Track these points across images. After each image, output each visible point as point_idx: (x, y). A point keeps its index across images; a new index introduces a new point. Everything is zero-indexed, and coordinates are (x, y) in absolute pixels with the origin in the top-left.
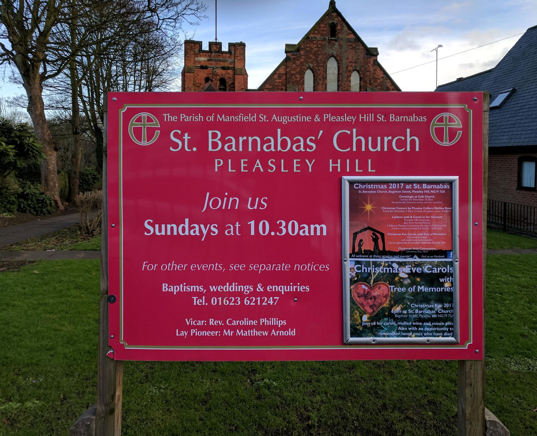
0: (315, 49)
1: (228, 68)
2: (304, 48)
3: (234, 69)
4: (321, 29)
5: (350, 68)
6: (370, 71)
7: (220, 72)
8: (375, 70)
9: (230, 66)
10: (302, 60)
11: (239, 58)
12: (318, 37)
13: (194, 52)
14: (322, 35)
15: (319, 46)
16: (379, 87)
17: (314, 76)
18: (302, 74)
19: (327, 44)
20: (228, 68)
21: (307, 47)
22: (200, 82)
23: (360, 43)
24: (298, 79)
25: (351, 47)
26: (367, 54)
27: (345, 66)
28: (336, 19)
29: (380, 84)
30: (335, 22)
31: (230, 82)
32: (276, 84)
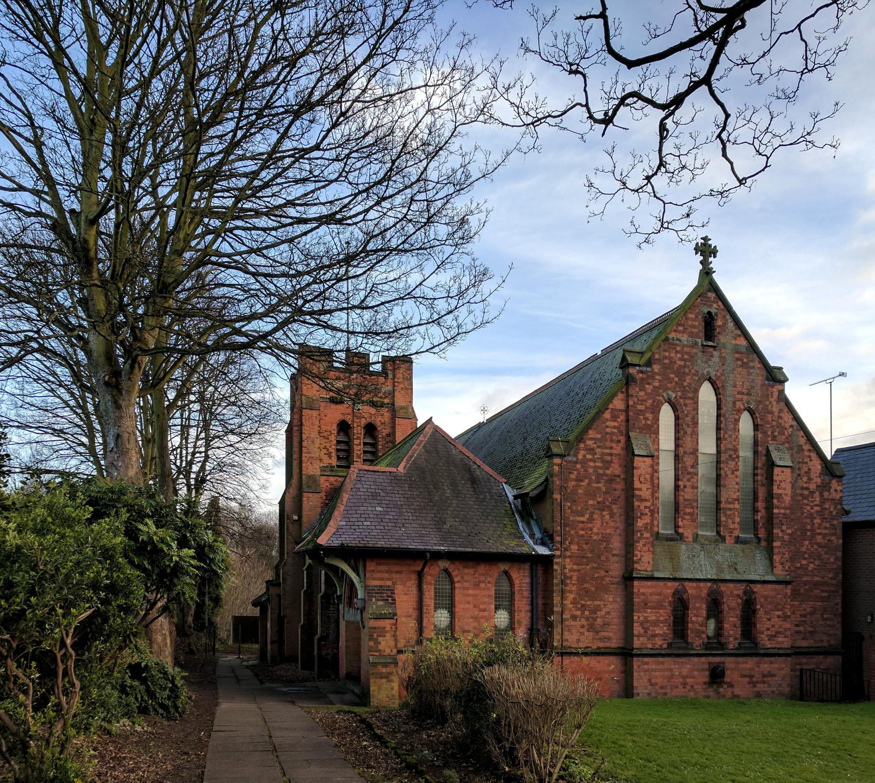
4: (690, 323)
5: (739, 405)
6: (772, 413)
8: (781, 411)
10: (657, 384)
11: (401, 386)
12: (684, 338)
14: (691, 335)
15: (686, 357)
16: (787, 445)
17: (677, 418)
18: (656, 411)
19: (700, 354)
21: (665, 357)
22: (328, 428)
24: (649, 422)
25: (740, 363)
26: (767, 379)
27: (730, 399)
28: (715, 306)
30: (713, 311)
31: (385, 432)
32: (608, 430)
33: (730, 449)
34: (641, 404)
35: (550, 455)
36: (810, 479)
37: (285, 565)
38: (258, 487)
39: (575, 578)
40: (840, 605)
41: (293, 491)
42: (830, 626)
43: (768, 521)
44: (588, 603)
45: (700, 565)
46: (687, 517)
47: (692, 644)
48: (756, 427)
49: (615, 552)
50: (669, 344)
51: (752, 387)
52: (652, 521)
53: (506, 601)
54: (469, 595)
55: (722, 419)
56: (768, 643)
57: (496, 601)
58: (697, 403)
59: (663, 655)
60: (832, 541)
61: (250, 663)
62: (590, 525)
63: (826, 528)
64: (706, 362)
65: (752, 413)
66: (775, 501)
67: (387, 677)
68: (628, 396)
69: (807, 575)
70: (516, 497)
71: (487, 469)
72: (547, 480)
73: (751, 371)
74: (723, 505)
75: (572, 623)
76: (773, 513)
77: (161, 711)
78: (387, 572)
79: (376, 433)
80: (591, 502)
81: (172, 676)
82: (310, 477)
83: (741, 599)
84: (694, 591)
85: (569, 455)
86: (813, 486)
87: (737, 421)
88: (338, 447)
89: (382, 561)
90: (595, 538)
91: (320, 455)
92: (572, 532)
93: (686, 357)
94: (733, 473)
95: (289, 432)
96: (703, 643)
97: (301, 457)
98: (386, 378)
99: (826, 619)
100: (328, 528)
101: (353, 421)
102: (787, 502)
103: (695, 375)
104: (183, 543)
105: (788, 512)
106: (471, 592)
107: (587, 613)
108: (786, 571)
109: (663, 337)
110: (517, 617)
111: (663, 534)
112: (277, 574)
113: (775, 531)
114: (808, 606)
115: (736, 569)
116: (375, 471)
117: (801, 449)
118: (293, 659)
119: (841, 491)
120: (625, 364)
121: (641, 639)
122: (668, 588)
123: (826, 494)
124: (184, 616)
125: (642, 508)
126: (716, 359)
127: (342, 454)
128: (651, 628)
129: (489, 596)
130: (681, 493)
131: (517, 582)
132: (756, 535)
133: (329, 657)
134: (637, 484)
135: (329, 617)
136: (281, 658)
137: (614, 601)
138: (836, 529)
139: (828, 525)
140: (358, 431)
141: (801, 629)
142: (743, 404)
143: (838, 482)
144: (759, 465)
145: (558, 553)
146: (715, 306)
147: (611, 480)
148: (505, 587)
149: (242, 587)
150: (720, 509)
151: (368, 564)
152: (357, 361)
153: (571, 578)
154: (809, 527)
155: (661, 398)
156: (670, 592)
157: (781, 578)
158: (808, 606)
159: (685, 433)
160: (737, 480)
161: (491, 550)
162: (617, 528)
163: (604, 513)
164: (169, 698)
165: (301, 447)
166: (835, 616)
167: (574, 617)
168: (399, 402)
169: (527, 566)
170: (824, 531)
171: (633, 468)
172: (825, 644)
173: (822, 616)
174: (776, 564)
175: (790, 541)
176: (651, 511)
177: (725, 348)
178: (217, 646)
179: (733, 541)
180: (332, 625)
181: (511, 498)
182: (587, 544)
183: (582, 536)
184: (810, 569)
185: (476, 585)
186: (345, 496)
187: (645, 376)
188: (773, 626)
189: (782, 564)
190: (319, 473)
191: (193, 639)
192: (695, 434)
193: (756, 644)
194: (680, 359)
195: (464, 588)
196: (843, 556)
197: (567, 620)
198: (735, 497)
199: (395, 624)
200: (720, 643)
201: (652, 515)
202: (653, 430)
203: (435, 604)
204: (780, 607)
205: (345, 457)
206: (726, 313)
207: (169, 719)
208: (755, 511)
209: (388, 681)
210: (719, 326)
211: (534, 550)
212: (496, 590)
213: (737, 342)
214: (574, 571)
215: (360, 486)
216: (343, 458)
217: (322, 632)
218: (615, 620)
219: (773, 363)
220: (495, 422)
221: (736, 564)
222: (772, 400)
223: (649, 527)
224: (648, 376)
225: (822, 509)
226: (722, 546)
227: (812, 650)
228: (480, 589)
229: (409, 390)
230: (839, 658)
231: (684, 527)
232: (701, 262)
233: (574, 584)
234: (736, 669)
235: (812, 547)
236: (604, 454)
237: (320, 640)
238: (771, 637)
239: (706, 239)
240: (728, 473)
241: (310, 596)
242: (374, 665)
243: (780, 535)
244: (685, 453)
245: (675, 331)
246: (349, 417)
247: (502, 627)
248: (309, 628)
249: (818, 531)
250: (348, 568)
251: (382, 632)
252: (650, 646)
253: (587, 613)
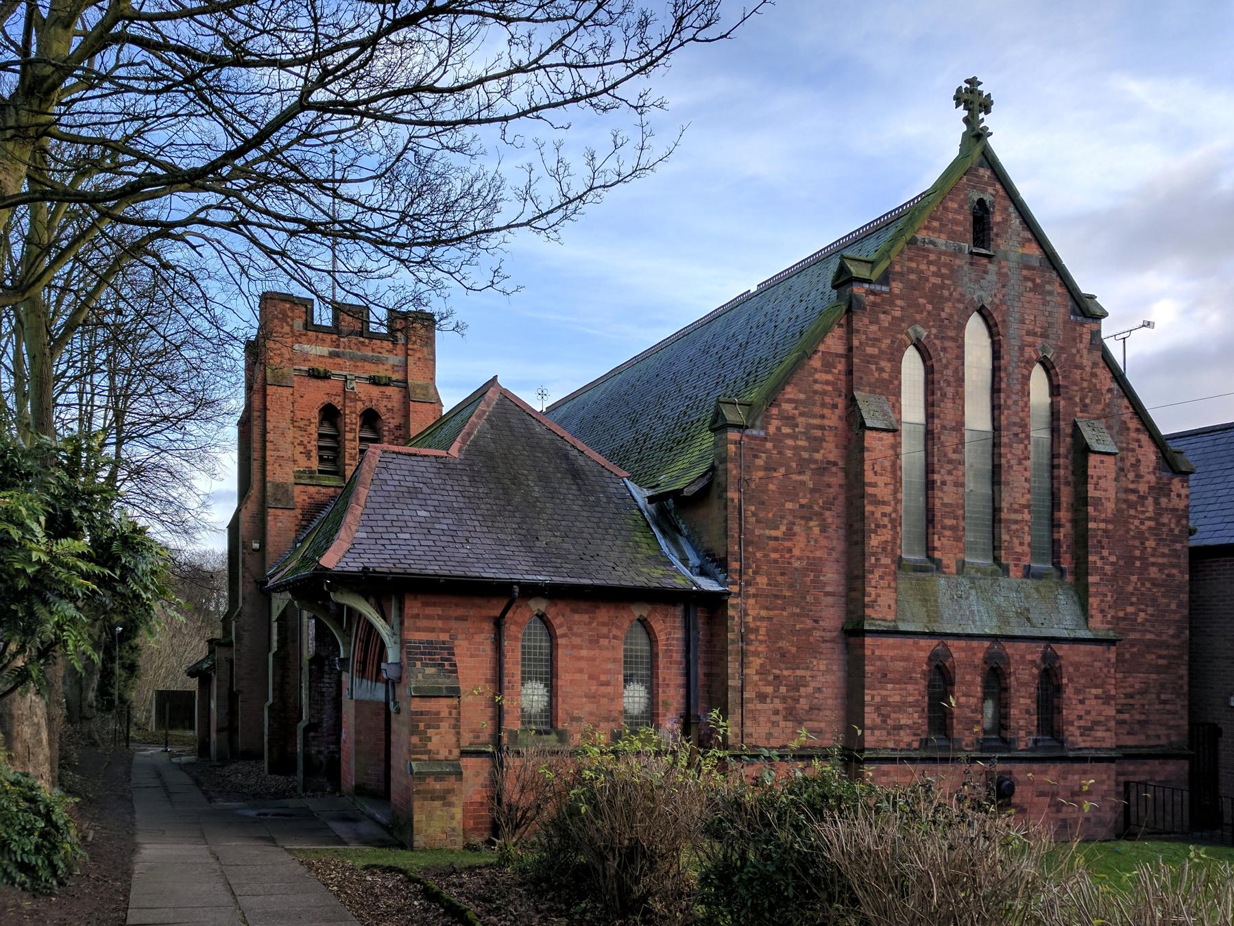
0: (933, 280)
1: (388, 383)
2: (902, 274)
3: (404, 385)
4: (950, 216)
5: (1029, 352)
6: (1080, 367)
7: (363, 390)
8: (1095, 365)
9: (394, 377)
10: (897, 313)
11: (418, 355)
12: (941, 241)
13: (292, 326)
14: (952, 236)
15: (944, 271)
19: (966, 268)
20: (388, 383)
21: (911, 271)
22: (307, 415)
23: (1054, 274)
24: (885, 376)
25: (1030, 284)
26: (1074, 312)
27: (1015, 343)
28: (990, 190)
30: (987, 198)
31: (394, 422)
32: (817, 387)
33: (1015, 424)
34: (873, 346)
35: (719, 425)
37: (239, 615)
38: (195, 505)
39: (763, 631)
40: (1186, 679)
41: (252, 506)
42: (1169, 712)
43: (1076, 542)
44: (786, 673)
45: (975, 609)
46: (948, 533)
47: (960, 741)
48: (1055, 390)
49: (828, 589)
50: (919, 249)
51: (1050, 325)
52: (894, 539)
53: (646, 670)
54: (580, 659)
55: (1003, 375)
56: (1080, 739)
57: (625, 669)
58: (961, 347)
59: (912, 760)
60: (1173, 576)
61: (184, 759)
62: (788, 544)
63: (1163, 555)
64: (977, 281)
65: (1048, 367)
66: (1091, 509)
67: (444, 797)
68: (850, 331)
69: (1134, 630)
70: (651, 500)
71: (595, 456)
72: (712, 468)
73: (1048, 298)
74: (1004, 515)
75: (759, 706)
76: (1087, 529)
77: (21, 877)
78: (440, 617)
79: (379, 424)
80: (789, 505)
81: (47, 806)
82: (278, 486)
83: (1037, 666)
84: (963, 654)
85: (753, 427)
86: (1143, 488)
87: (1026, 379)
88: (321, 444)
89: (432, 599)
90: (797, 564)
91: (292, 455)
92: (759, 555)
93: (944, 271)
94: (1020, 464)
95: (245, 425)
96: (978, 740)
97: (264, 457)
98: (395, 343)
99: (1165, 702)
100: (336, 543)
101: (344, 405)
102: (1109, 511)
103: (959, 301)
105: (1110, 527)
106: (584, 653)
107: (783, 689)
108: (1108, 623)
109: (908, 236)
110: (661, 696)
111: (907, 560)
113: (1091, 558)
114: (1135, 681)
115: (1028, 619)
116: (410, 455)
117: (1124, 428)
118: (253, 755)
119: (1187, 496)
120: (843, 279)
121: (877, 733)
122: (921, 649)
123: (1164, 501)
124: (81, 690)
125: (878, 515)
126: (992, 277)
127: (326, 454)
128: (893, 715)
129: (615, 661)
130: (938, 493)
131: (661, 637)
132: (1057, 565)
133: (321, 757)
134: (869, 477)
135: (322, 694)
136: (232, 754)
137: (828, 671)
138: (1179, 557)
139: (1166, 551)
140: (352, 420)
141: (1126, 716)
142: (1036, 351)
143: (1183, 481)
144: (1062, 451)
145: (735, 589)
146: (990, 190)
147: (823, 469)
148: (641, 645)
149: (170, 648)
150: (1000, 521)
151: (408, 603)
153: (757, 630)
154: (1137, 553)
155: (904, 336)
156: (924, 655)
157: (1101, 635)
158: (1135, 681)
159: (944, 395)
160: (1027, 474)
161: (623, 583)
162: (833, 549)
163: (812, 524)
164: (38, 849)
165: (264, 442)
166: (1178, 696)
167: (762, 697)
168: (415, 378)
169: (679, 611)
170: (1160, 560)
171: (862, 449)
172: (1163, 741)
173: (1159, 697)
174: (1093, 612)
175: (1114, 575)
176: (892, 521)
177: (1007, 259)
178: (132, 734)
179: (1019, 574)
180: (328, 708)
181: (642, 502)
182: (782, 574)
183: (776, 561)
184: (1139, 620)
185: (594, 642)
186: (363, 492)
187: (878, 300)
188: (1088, 713)
189: (1102, 611)
190: (292, 480)
191: (95, 725)
192: (959, 397)
193: (1062, 742)
194: (935, 274)
195: (574, 647)
196: (1191, 600)
197: (751, 700)
198: (1023, 501)
199: (457, 708)
200: (1004, 740)
201: (894, 527)
202: (891, 387)
203: (523, 672)
204: (1098, 682)
205: (332, 455)
206: (1008, 203)
207: (35, 893)
208: (1054, 525)
209: (444, 805)
210: (998, 223)
211: (695, 584)
212: (625, 650)
213: (1026, 251)
214: (762, 619)
215: (385, 476)
216: (328, 460)
217: (311, 716)
218: (830, 702)
219: (1084, 288)
220: (564, 408)
221: (1028, 610)
222: (1081, 346)
223: (889, 548)
224: (883, 300)
225: (1158, 524)
226: (1003, 581)
227: (1144, 751)
228: (600, 648)
229: (430, 361)
230: (1185, 765)
231: (943, 548)
232: (966, 120)
233: (761, 642)
234: (1030, 779)
235: (1143, 585)
236: (810, 427)
237: (306, 730)
238: (1085, 731)
239: (973, 82)
240: (1013, 462)
241: (283, 660)
242: (422, 776)
243: (1099, 564)
244: (944, 427)
245: (926, 228)
246: (339, 399)
247: (636, 712)
248: (285, 713)
249: (1152, 560)
250: (372, 610)
251: (434, 720)
252: (891, 745)
253: (783, 689)
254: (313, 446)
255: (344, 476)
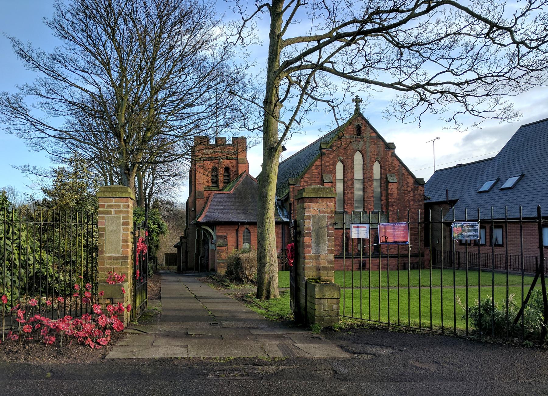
5: (373, 159)
8: (393, 160)
14: (350, 134)
16: (396, 174)
17: (344, 167)
18: (334, 165)
26: (386, 148)
29: (397, 171)
31: (234, 170)
36: (408, 186)
41: (192, 198)
66: (389, 196)
82: (200, 192)
86: (409, 189)
91: (204, 180)
104: (154, 224)
112: (185, 233)
120: (321, 148)
123: (416, 192)
152: (221, 142)
168: (240, 157)
169: (281, 226)
180: (206, 252)
202: (334, 172)
208: (381, 200)
234: (371, 262)
240: (368, 186)
241: (198, 241)
242: (219, 263)
248: (197, 255)
254: (210, 179)
255: (219, 187)
